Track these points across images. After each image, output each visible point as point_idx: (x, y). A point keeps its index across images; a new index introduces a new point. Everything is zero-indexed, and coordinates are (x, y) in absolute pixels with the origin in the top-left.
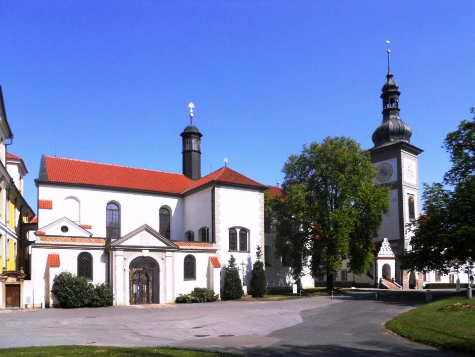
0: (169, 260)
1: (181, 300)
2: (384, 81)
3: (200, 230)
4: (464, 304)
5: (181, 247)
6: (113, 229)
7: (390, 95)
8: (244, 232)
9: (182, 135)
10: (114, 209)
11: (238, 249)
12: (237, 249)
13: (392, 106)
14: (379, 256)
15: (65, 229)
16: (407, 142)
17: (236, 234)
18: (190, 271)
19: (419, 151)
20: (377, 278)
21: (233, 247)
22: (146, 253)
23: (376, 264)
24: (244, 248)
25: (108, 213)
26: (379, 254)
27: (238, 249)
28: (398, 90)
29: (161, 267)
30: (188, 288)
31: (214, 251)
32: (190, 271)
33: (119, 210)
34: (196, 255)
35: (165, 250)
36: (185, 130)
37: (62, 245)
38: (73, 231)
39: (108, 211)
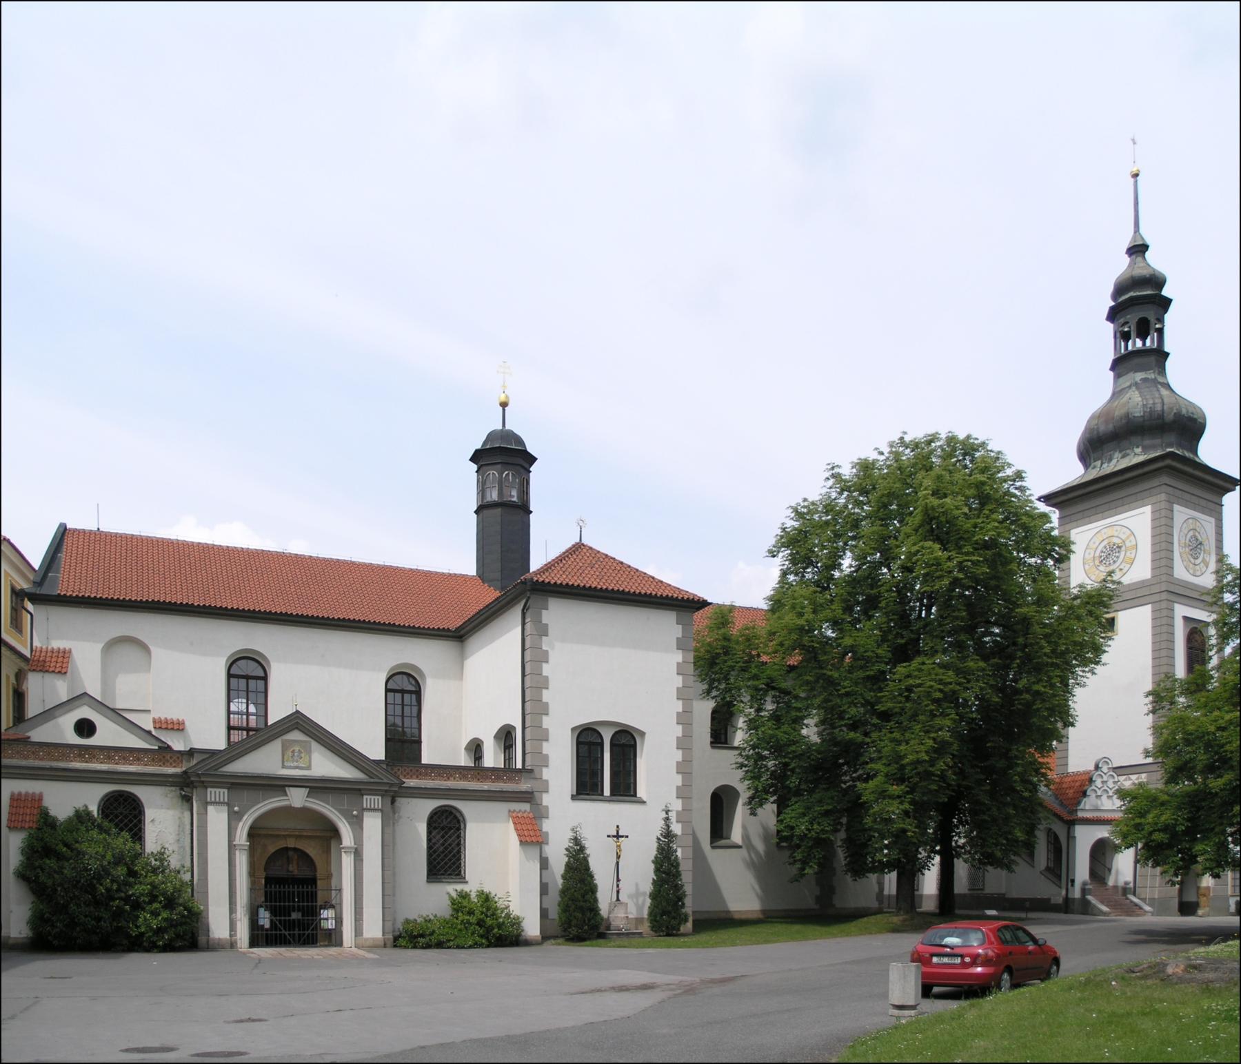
0: (373, 824)
1: (411, 937)
2: (1120, 265)
3: (497, 737)
4: (1166, 980)
5: (411, 783)
6: (403, 742)
7: (1140, 305)
8: (627, 742)
9: (476, 457)
10: (404, 691)
11: (607, 792)
12: (602, 794)
13: (1144, 344)
14: (1080, 814)
15: (85, 728)
16: (1188, 454)
17: (602, 745)
18: (445, 858)
19: (1228, 485)
20: (1073, 881)
21: (587, 786)
22: (297, 798)
23: (1071, 838)
24: (625, 788)
25: (390, 700)
26: (1081, 807)
27: (607, 792)
28: (1166, 292)
29: (347, 839)
30: (432, 901)
31: (527, 797)
33: (418, 693)
34: (466, 808)
35: (360, 790)
36: (485, 443)
37: (51, 769)
38: (108, 734)
39: (390, 695)
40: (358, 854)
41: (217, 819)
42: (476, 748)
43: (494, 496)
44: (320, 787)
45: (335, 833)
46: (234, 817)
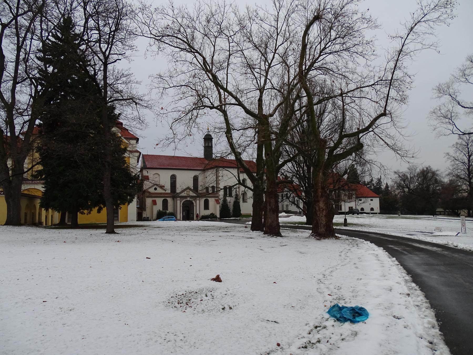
0: (198, 201)
15: (156, 189)
18: (206, 207)
22: (188, 199)
29: (195, 204)
31: (218, 197)
32: (206, 207)
34: (209, 199)
40: (196, 206)
41: (178, 202)
42: (207, 188)
43: (207, 145)
44: (192, 197)
45: (193, 203)
46: (181, 202)
